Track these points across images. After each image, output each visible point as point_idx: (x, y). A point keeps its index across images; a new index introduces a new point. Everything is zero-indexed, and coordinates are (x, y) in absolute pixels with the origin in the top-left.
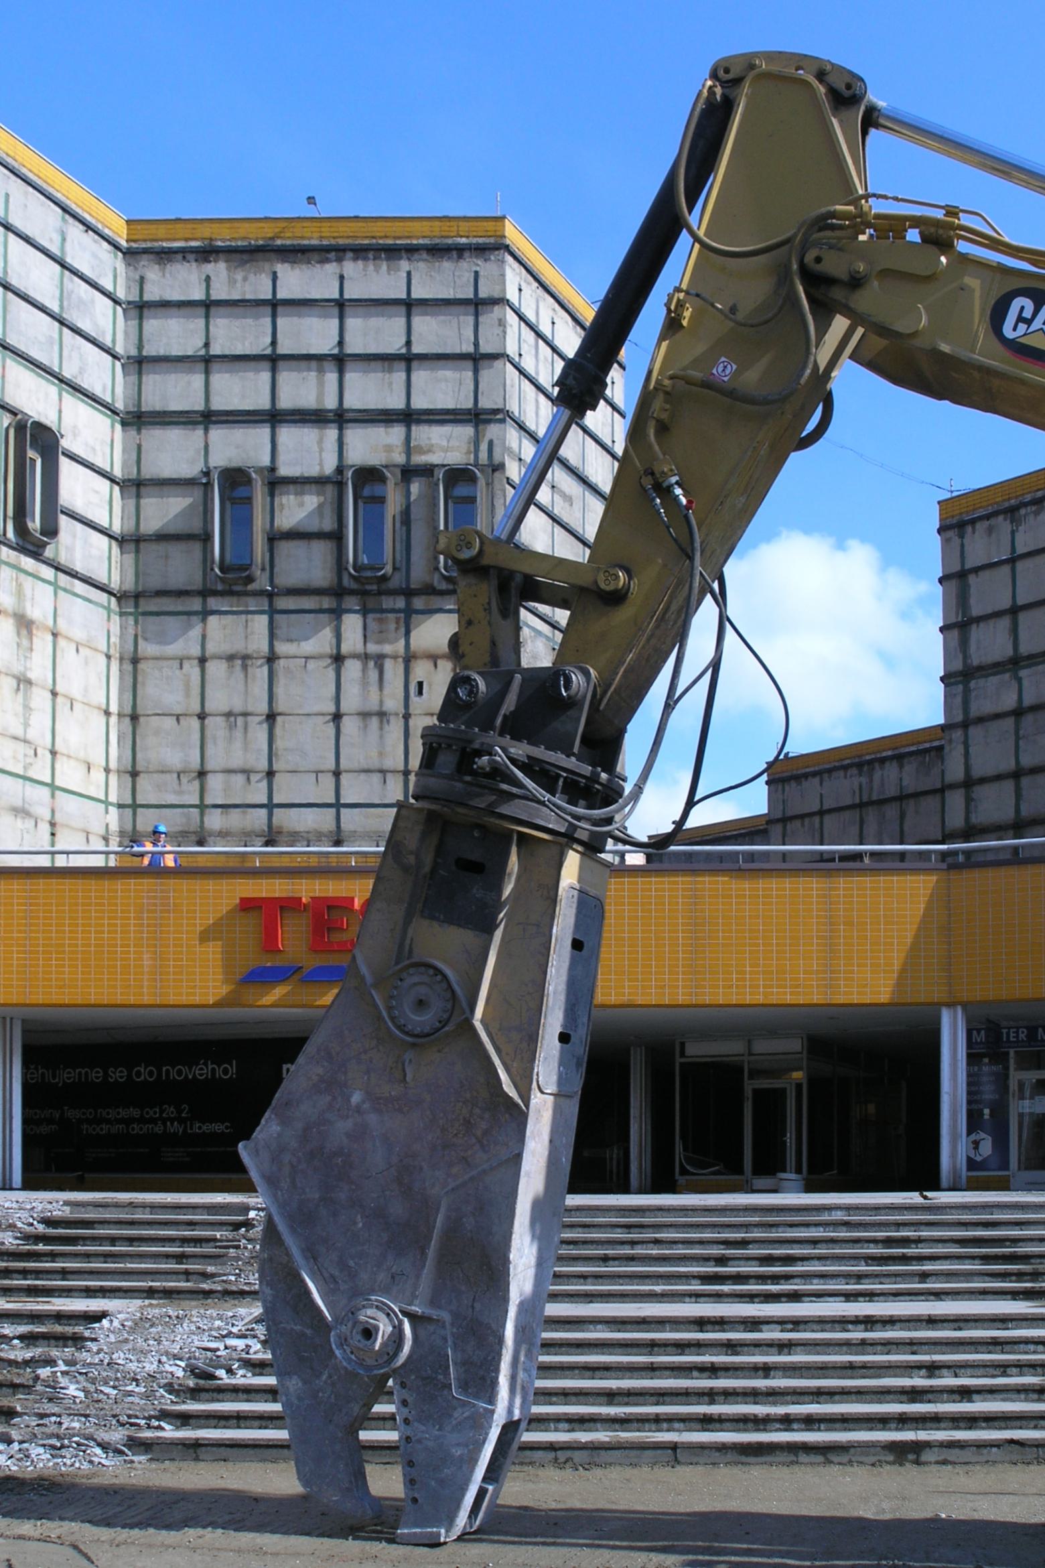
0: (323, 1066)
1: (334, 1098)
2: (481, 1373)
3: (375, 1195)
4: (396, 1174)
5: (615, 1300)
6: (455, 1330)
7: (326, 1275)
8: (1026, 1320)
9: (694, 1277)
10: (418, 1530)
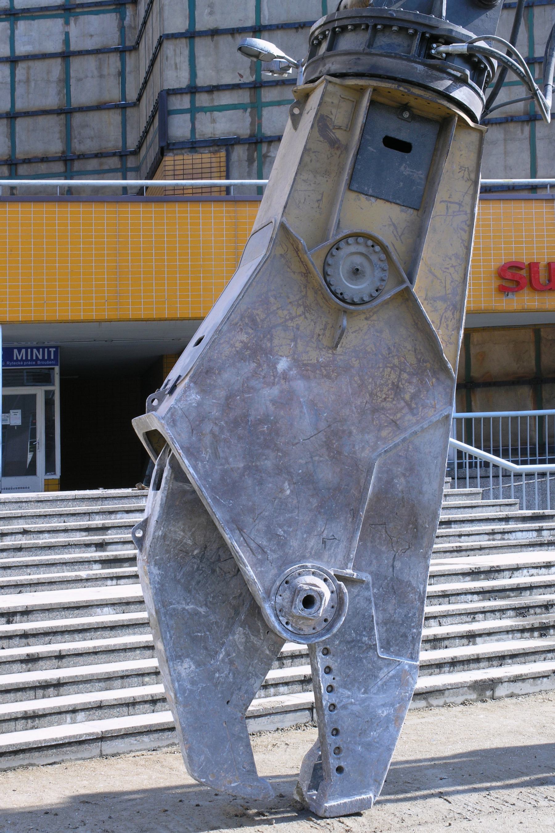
0: (247, 333)
1: (259, 365)
2: (403, 630)
3: (302, 461)
4: (324, 440)
5: (43, 588)
6: (375, 591)
7: (253, 545)
8: (443, 575)
9: (96, 562)
10: (346, 800)
